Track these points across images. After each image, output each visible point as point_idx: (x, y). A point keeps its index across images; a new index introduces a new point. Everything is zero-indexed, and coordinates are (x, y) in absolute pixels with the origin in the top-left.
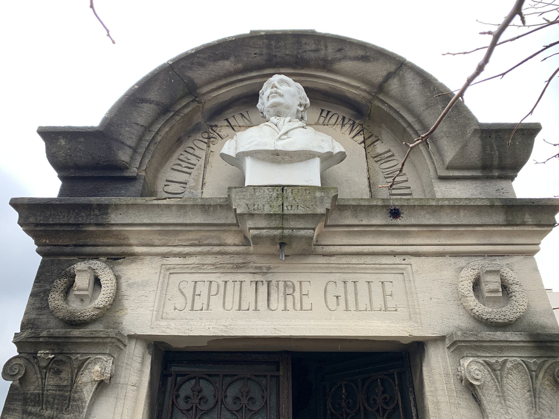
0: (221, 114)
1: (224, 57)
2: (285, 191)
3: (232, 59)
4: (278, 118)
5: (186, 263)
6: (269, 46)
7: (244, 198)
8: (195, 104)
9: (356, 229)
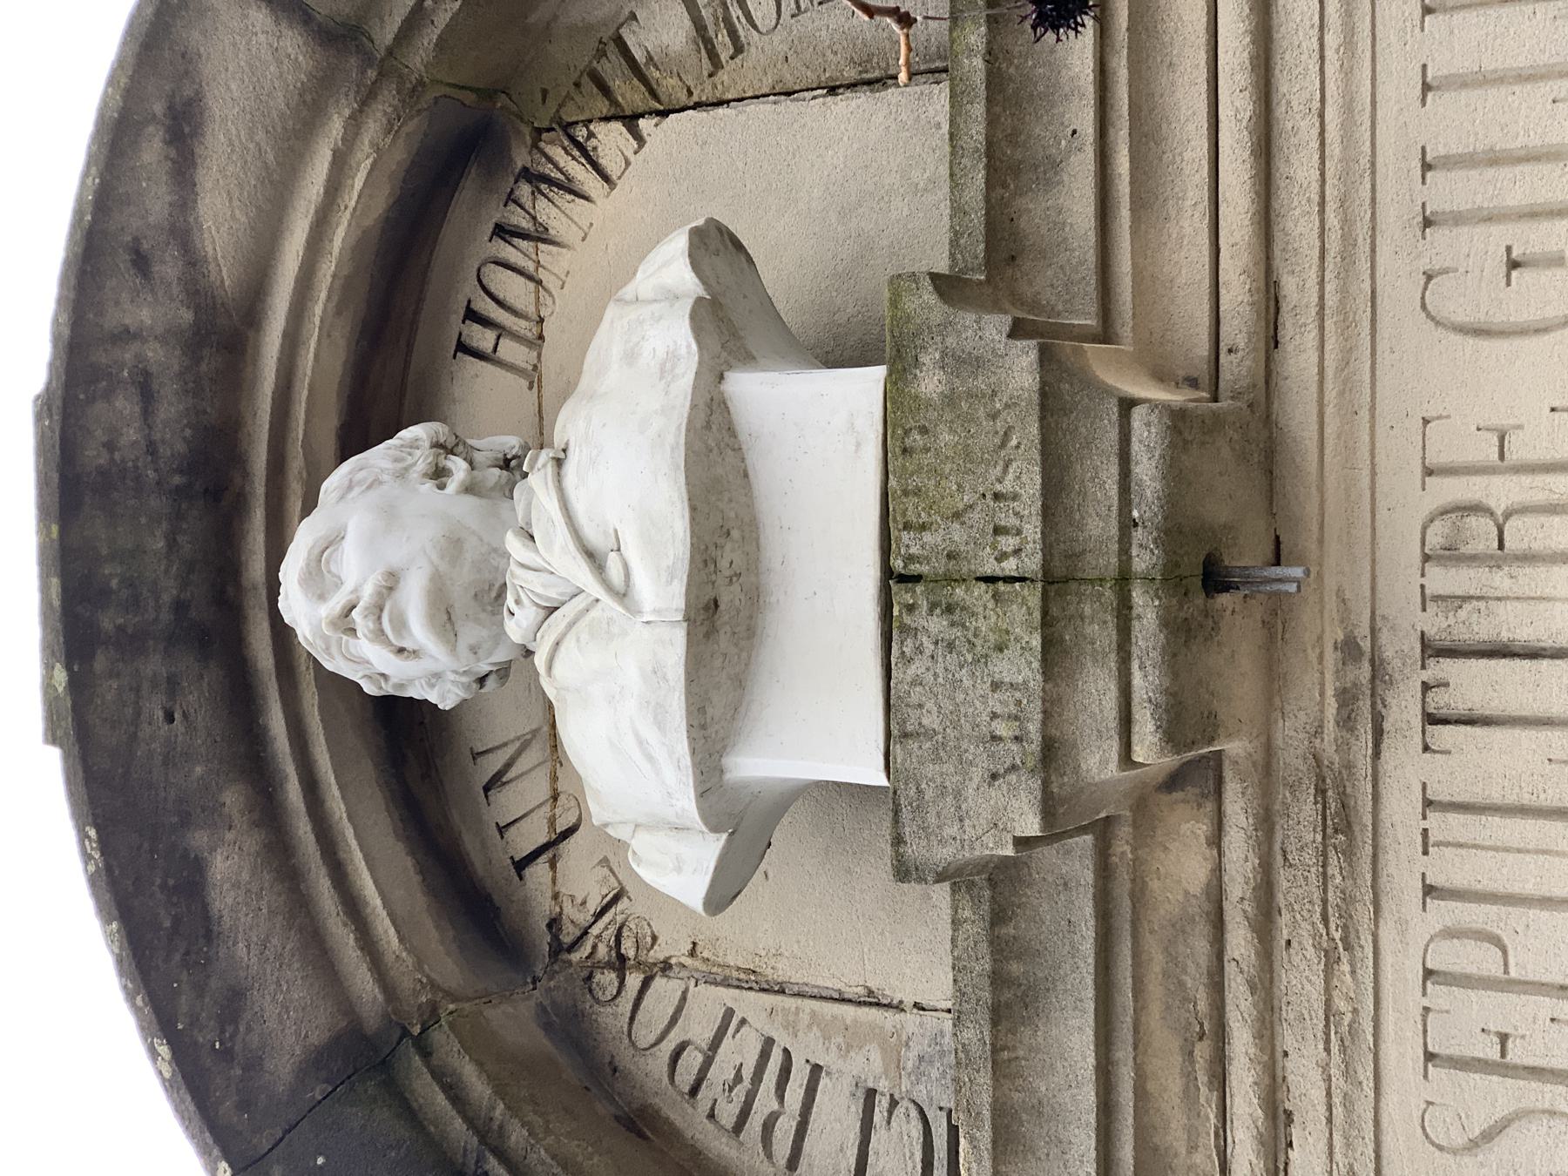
0: (488, 898)
1: (190, 883)
2: (915, 568)
3: (199, 839)
4: (510, 601)
5: (1322, 1109)
6: (131, 643)
7: (958, 794)
8: (443, 1040)
9: (1122, 163)
